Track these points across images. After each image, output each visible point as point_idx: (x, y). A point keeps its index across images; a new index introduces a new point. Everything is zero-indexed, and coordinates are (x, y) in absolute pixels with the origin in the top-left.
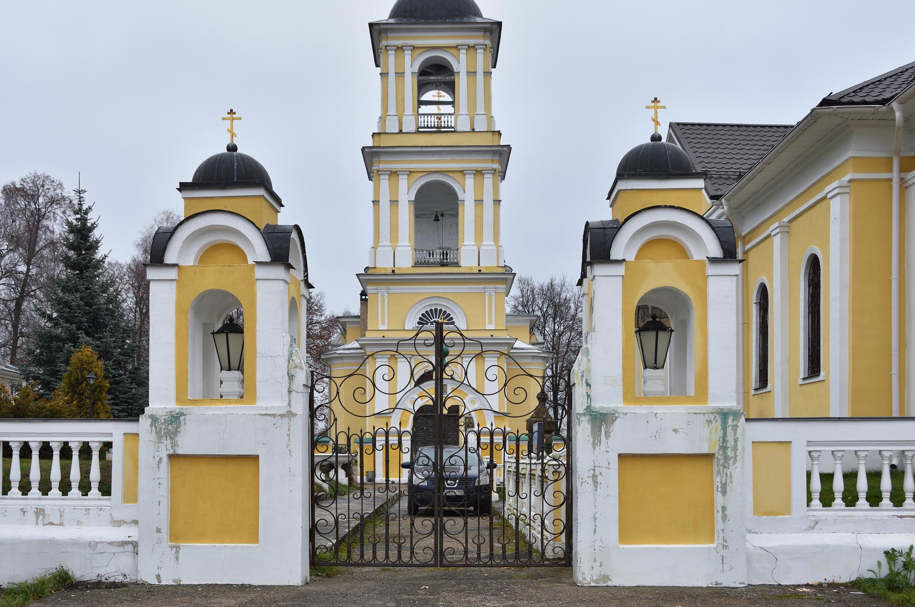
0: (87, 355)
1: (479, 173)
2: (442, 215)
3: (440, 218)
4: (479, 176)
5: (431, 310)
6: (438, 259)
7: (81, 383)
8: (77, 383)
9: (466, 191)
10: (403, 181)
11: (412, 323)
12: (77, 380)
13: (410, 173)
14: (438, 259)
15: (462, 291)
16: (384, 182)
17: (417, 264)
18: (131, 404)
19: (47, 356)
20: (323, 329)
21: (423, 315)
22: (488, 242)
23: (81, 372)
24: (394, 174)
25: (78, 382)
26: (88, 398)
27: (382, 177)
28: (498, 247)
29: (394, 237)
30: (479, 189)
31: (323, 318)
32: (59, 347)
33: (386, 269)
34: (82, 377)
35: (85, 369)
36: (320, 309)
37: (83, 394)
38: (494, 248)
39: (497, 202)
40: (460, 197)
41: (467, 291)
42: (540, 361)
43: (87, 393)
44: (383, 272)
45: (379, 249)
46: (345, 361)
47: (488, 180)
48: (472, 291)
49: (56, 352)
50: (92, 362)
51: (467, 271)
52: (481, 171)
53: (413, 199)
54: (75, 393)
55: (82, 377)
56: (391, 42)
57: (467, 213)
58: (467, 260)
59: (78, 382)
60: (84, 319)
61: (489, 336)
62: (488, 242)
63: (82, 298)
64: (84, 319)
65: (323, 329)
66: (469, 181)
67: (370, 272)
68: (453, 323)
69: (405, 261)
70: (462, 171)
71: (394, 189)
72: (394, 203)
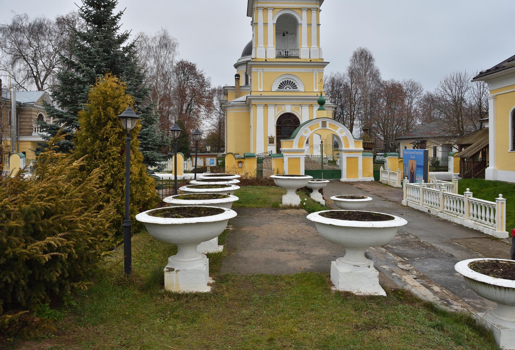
0: (111, 87)
1: (309, 10)
2: (287, 33)
3: (286, 34)
4: (309, 11)
5: (285, 81)
6: (286, 55)
7: (105, 124)
8: (98, 124)
9: (303, 19)
10: (270, 13)
11: (275, 88)
12: (99, 119)
13: (274, 9)
14: (286, 55)
15: (301, 71)
16: (260, 14)
17: (277, 57)
18: (145, 139)
19: (71, 98)
20: (210, 93)
21: (281, 83)
22: (314, 46)
23: (104, 109)
24: (265, 9)
25: (100, 123)
26: (115, 145)
27: (259, 11)
28: (320, 49)
29: (266, 43)
30: (309, 18)
31: (210, 89)
32: (80, 89)
33: (262, 59)
34: (106, 115)
35: (108, 105)
36: (209, 85)
37: (107, 139)
38: (318, 49)
39: (318, 25)
40: (300, 22)
41: (304, 71)
42: (331, 109)
43: (113, 138)
44: (260, 60)
45: (258, 48)
46: (235, 108)
47: (314, 14)
48: (307, 71)
49: (78, 93)
50: (119, 96)
51: (304, 61)
52: (266, 8)
53: (275, 22)
54: (96, 137)
55: (106, 115)
56: (259, 5)
57: (303, 31)
58: (304, 56)
59: (100, 123)
60: (103, 64)
61: (316, 95)
62: (314, 46)
63: (101, 46)
64: (103, 64)
65: (210, 93)
66: (304, 14)
67: (254, 60)
68: (297, 88)
69: (272, 55)
70: (301, 9)
71: (265, 17)
72: (266, 24)
